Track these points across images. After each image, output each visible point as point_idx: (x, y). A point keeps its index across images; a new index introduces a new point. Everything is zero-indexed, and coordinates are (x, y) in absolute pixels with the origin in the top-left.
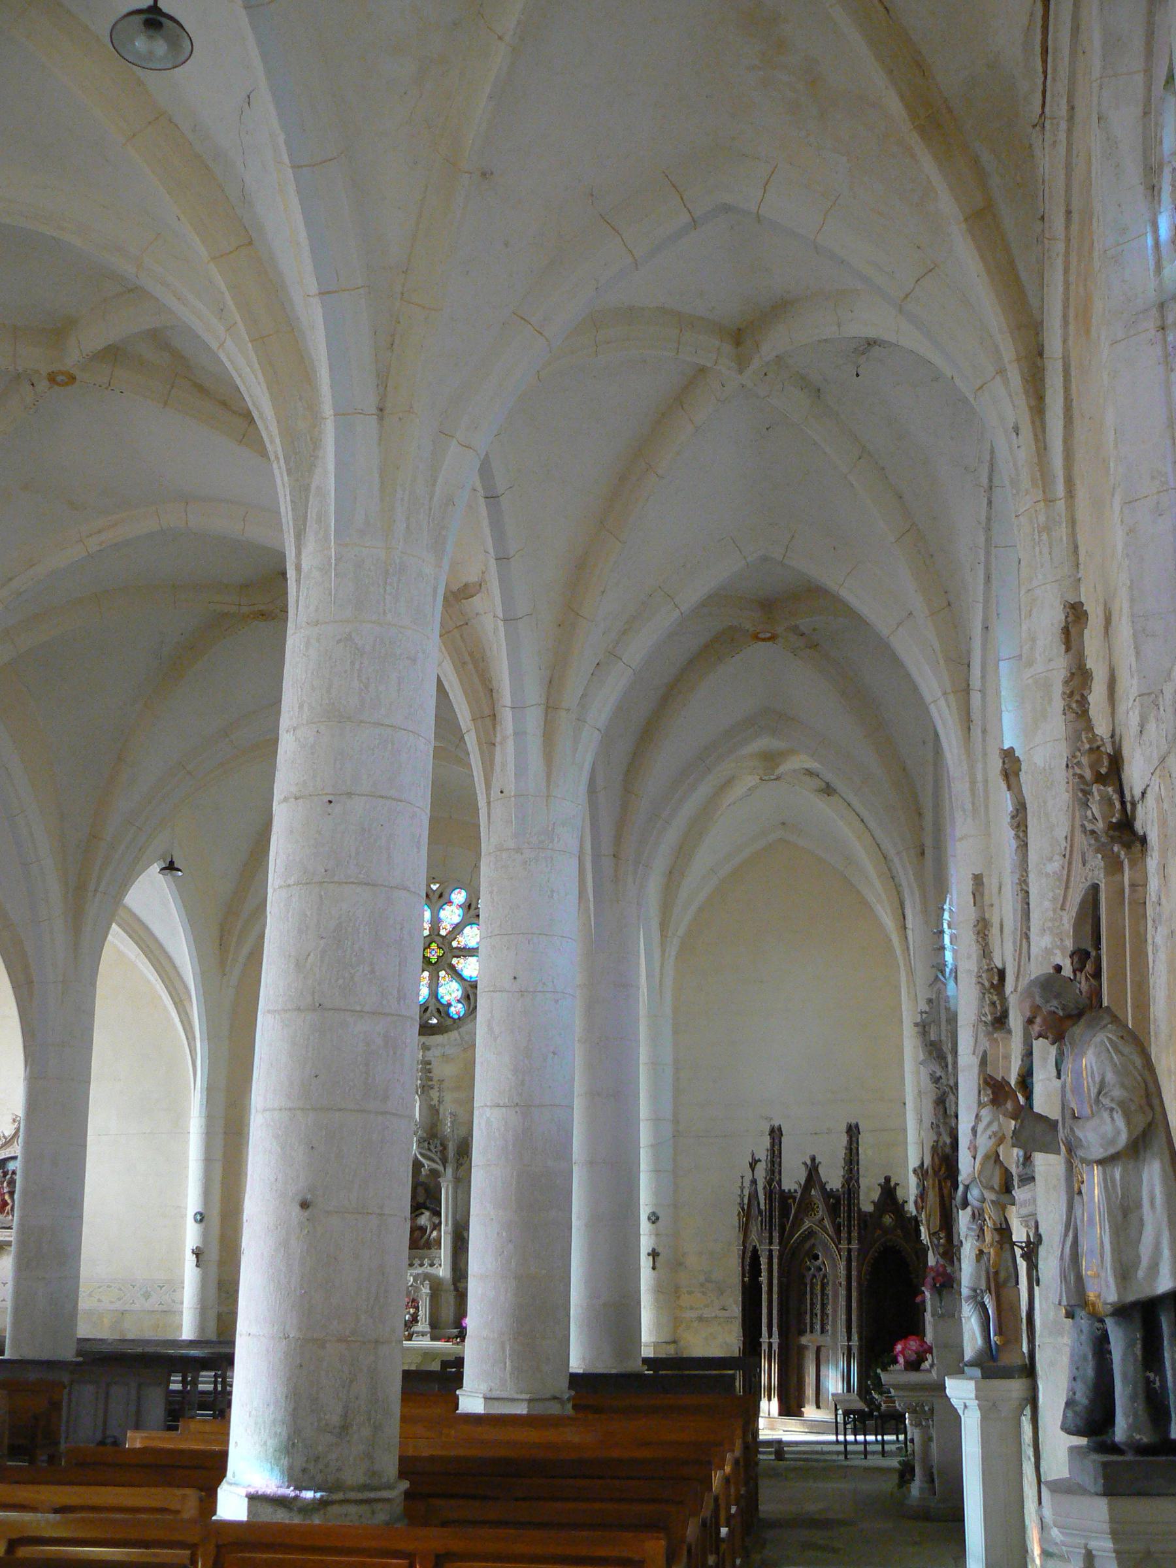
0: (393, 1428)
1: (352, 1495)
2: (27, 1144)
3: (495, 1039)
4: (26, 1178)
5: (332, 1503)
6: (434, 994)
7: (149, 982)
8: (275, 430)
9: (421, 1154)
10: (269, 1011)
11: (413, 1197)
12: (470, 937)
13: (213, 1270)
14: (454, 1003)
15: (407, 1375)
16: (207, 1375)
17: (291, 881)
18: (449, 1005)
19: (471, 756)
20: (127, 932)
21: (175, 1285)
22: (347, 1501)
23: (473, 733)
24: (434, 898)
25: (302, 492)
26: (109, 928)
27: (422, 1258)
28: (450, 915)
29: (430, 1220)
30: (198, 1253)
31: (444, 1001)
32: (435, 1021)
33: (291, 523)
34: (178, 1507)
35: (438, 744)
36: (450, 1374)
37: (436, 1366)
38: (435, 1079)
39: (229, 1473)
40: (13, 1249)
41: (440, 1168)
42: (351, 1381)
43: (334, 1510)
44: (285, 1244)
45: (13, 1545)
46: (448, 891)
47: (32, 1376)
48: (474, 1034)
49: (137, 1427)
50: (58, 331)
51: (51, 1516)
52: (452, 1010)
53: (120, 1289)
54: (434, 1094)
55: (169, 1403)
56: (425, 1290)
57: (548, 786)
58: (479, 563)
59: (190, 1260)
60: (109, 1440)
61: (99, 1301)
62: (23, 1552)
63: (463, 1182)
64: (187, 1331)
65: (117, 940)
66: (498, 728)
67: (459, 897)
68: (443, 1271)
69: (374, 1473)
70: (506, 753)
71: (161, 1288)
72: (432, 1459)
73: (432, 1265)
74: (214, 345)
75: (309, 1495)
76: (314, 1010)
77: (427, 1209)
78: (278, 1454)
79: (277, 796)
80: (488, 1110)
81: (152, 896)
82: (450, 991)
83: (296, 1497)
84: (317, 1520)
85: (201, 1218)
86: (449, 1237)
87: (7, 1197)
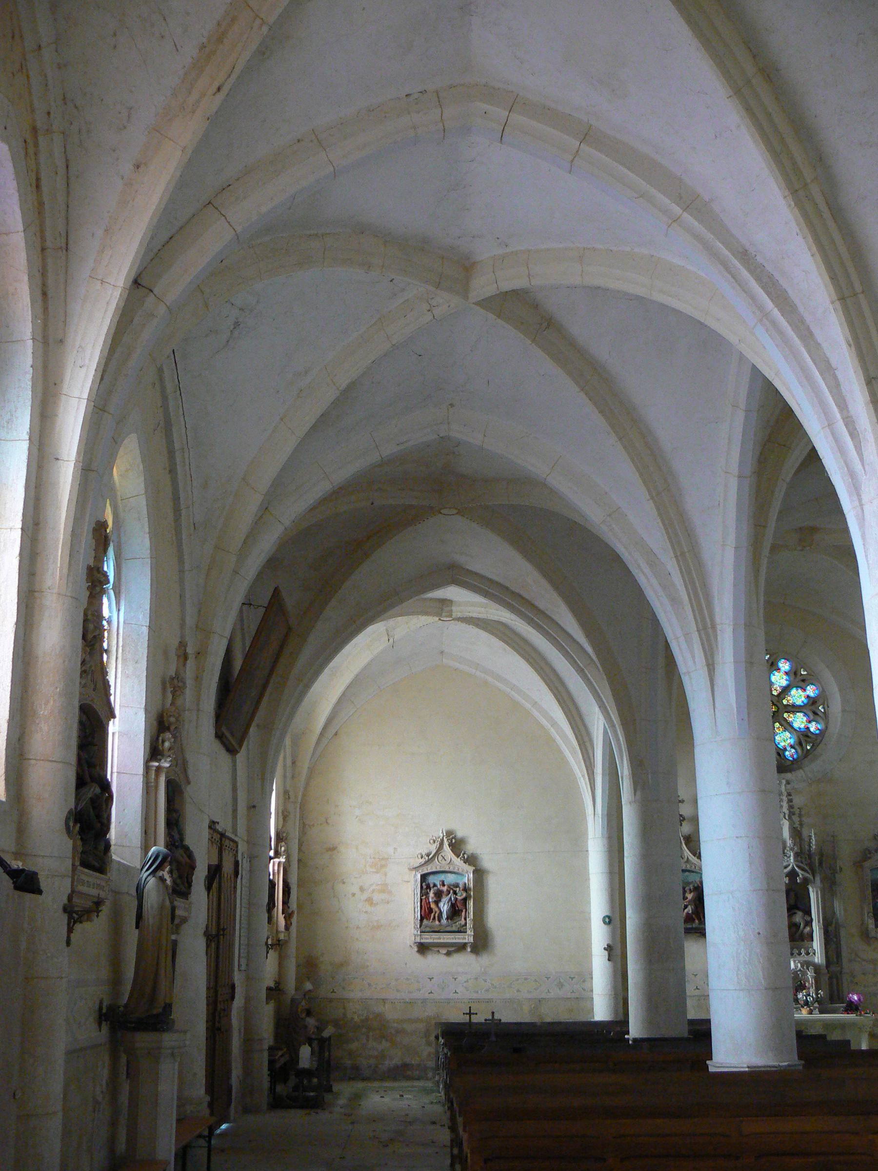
7: (542, 727)
9: (798, 866)
13: (619, 960)
14: (788, 749)
18: (785, 749)
21: (586, 976)
24: (799, 678)
29: (803, 918)
41: (810, 876)
53: (536, 981)
54: (796, 818)
56: (810, 974)
61: (518, 991)
71: (572, 979)
77: (799, 909)
87: (433, 906)
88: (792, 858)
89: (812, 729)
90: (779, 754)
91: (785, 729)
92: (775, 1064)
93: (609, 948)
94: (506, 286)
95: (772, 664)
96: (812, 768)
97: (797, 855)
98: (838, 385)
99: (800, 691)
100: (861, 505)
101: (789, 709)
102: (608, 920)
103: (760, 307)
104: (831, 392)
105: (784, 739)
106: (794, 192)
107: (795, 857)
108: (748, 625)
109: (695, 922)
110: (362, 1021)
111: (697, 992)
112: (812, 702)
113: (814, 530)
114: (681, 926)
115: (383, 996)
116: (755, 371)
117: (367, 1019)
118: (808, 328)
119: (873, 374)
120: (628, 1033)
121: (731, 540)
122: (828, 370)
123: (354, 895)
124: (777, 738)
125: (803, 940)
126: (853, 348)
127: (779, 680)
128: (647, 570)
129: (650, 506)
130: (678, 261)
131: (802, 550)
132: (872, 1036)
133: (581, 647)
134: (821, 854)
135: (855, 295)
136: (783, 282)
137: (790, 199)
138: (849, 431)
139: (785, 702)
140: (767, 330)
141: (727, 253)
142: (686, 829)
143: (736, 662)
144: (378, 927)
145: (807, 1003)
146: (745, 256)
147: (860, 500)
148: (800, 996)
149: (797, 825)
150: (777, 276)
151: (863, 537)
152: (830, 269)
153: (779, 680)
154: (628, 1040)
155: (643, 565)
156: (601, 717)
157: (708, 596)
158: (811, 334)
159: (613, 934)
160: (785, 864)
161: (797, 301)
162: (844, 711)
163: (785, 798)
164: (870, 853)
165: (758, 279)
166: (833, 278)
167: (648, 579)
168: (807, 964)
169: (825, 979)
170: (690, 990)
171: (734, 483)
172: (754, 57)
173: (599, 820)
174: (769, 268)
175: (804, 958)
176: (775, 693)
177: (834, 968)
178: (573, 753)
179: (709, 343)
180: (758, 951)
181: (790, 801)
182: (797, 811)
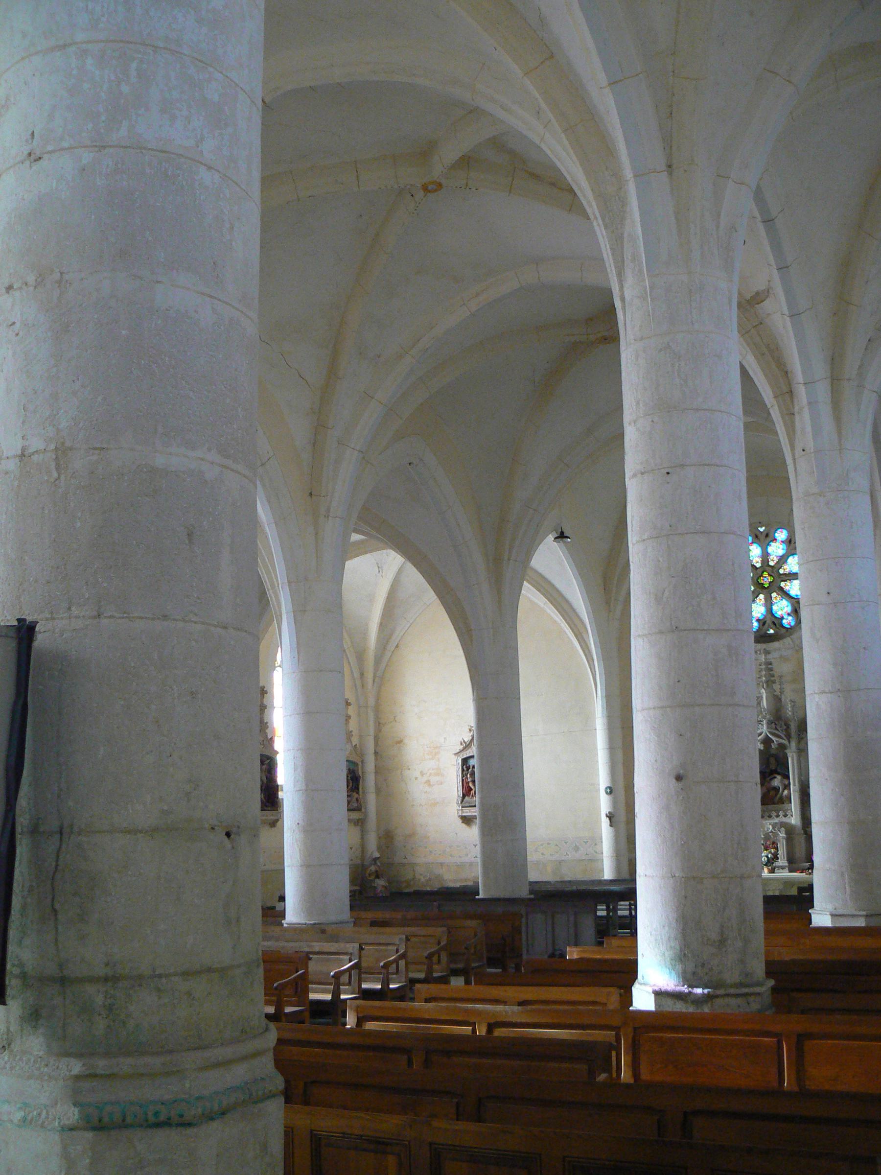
0: (759, 941)
1: (732, 991)
2: (480, 747)
3: (817, 641)
4: (482, 772)
5: (717, 996)
6: (770, 611)
7: (555, 622)
8: (591, 197)
10: (639, 636)
12: (792, 565)
13: (622, 826)
14: (785, 616)
15: (769, 901)
16: (624, 904)
17: (645, 537)
18: (782, 618)
19: (777, 425)
20: (534, 586)
21: (596, 841)
22: (727, 995)
23: (776, 407)
24: (762, 537)
25: (618, 241)
26: (522, 584)
27: (777, 811)
28: (776, 550)
29: (781, 781)
30: (610, 816)
32: (772, 631)
33: (612, 266)
34: (605, 1001)
35: (750, 419)
36: (804, 898)
37: (794, 892)
38: (776, 675)
39: (639, 976)
40: (478, 821)
41: (786, 742)
42: (724, 909)
43: (719, 1001)
44: (667, 808)
45: (491, 1027)
46: (773, 531)
47: (499, 910)
48: (801, 638)
49: (576, 944)
50: (425, 152)
51: (516, 1008)
52: (784, 621)
54: (777, 687)
55: (597, 925)
56: (782, 835)
57: (840, 439)
58: (765, 274)
59: (605, 822)
60: (557, 953)
61: (543, 854)
62: (499, 1032)
63: (803, 752)
64: (608, 873)
65: (529, 593)
66: (795, 400)
67: (782, 535)
68: (795, 820)
69: (747, 975)
70: (804, 420)
72: (794, 962)
73: (785, 816)
74: (537, 140)
75: (699, 991)
76: (673, 631)
77: (779, 774)
78: (673, 962)
79: (628, 475)
80: (816, 696)
81: (551, 559)
82: (782, 607)
83: (690, 992)
84: (706, 1009)
85: (610, 791)
86: (797, 795)
87: (471, 785)
101: (784, 578)
110: (427, 881)
115: (441, 860)
117: (430, 880)
123: (416, 778)
144: (435, 804)
160: (759, 732)
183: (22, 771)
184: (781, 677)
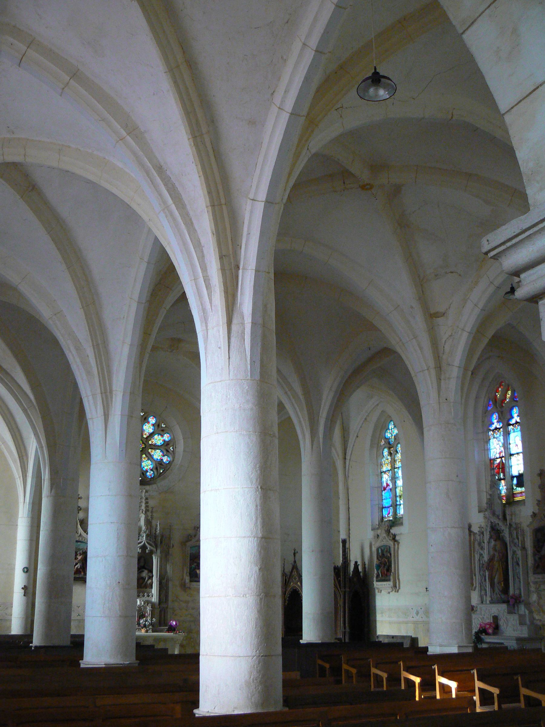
9: (147, 543)
11: (138, 563)
18: (147, 471)
21: (8, 606)
24: (160, 429)
27: (144, 593)
31: (144, 469)
41: (155, 549)
54: (149, 514)
56: (149, 608)
77: (146, 569)
88: (144, 537)
89: (164, 461)
90: (143, 473)
91: (148, 459)
92: (122, 662)
93: (25, 588)
94: (9, 159)
95: (145, 419)
96: (162, 484)
97: (147, 536)
98: (203, 256)
99: (160, 436)
100: (207, 330)
101: (153, 447)
102: (26, 570)
103: (165, 202)
104: (198, 260)
105: (147, 465)
106: (194, 137)
107: (146, 537)
108: (132, 393)
109: (81, 575)
111: (79, 618)
112: (166, 444)
113: (179, 340)
114: (72, 576)
116: (156, 239)
118: (191, 219)
119: (224, 253)
120: (32, 643)
121: (128, 340)
122: (198, 245)
124: (143, 464)
125: (146, 588)
126: (215, 236)
127: (148, 428)
128: (74, 352)
129: (81, 312)
130: (120, 165)
131: (171, 352)
132: (182, 646)
133: (27, 395)
134: (162, 536)
135: (221, 205)
136: (180, 189)
137: (191, 140)
138: (206, 284)
139: (150, 442)
140: (166, 216)
141: (149, 165)
142: (81, 515)
143: (122, 415)
145: (145, 626)
146: (160, 169)
147: (207, 326)
148: (141, 621)
149: (149, 518)
150: (177, 184)
151: (206, 349)
152: (208, 186)
153: (148, 428)
154: (32, 646)
155: (72, 348)
156: (35, 441)
157: (110, 373)
158: (192, 223)
159: (28, 579)
161: (186, 202)
162: (184, 451)
163: (144, 500)
164: (191, 537)
165: (166, 185)
166: (209, 193)
167: (74, 358)
168: (147, 602)
169: (157, 611)
170: (74, 616)
171: (134, 306)
172: (184, 52)
173: (27, 506)
174: (173, 179)
175: (146, 598)
176: (145, 436)
177: (162, 606)
178: (14, 462)
179: (131, 218)
180: (118, 593)
181: (147, 503)
182: (150, 509)
183: (41, 512)
184: (152, 508)
